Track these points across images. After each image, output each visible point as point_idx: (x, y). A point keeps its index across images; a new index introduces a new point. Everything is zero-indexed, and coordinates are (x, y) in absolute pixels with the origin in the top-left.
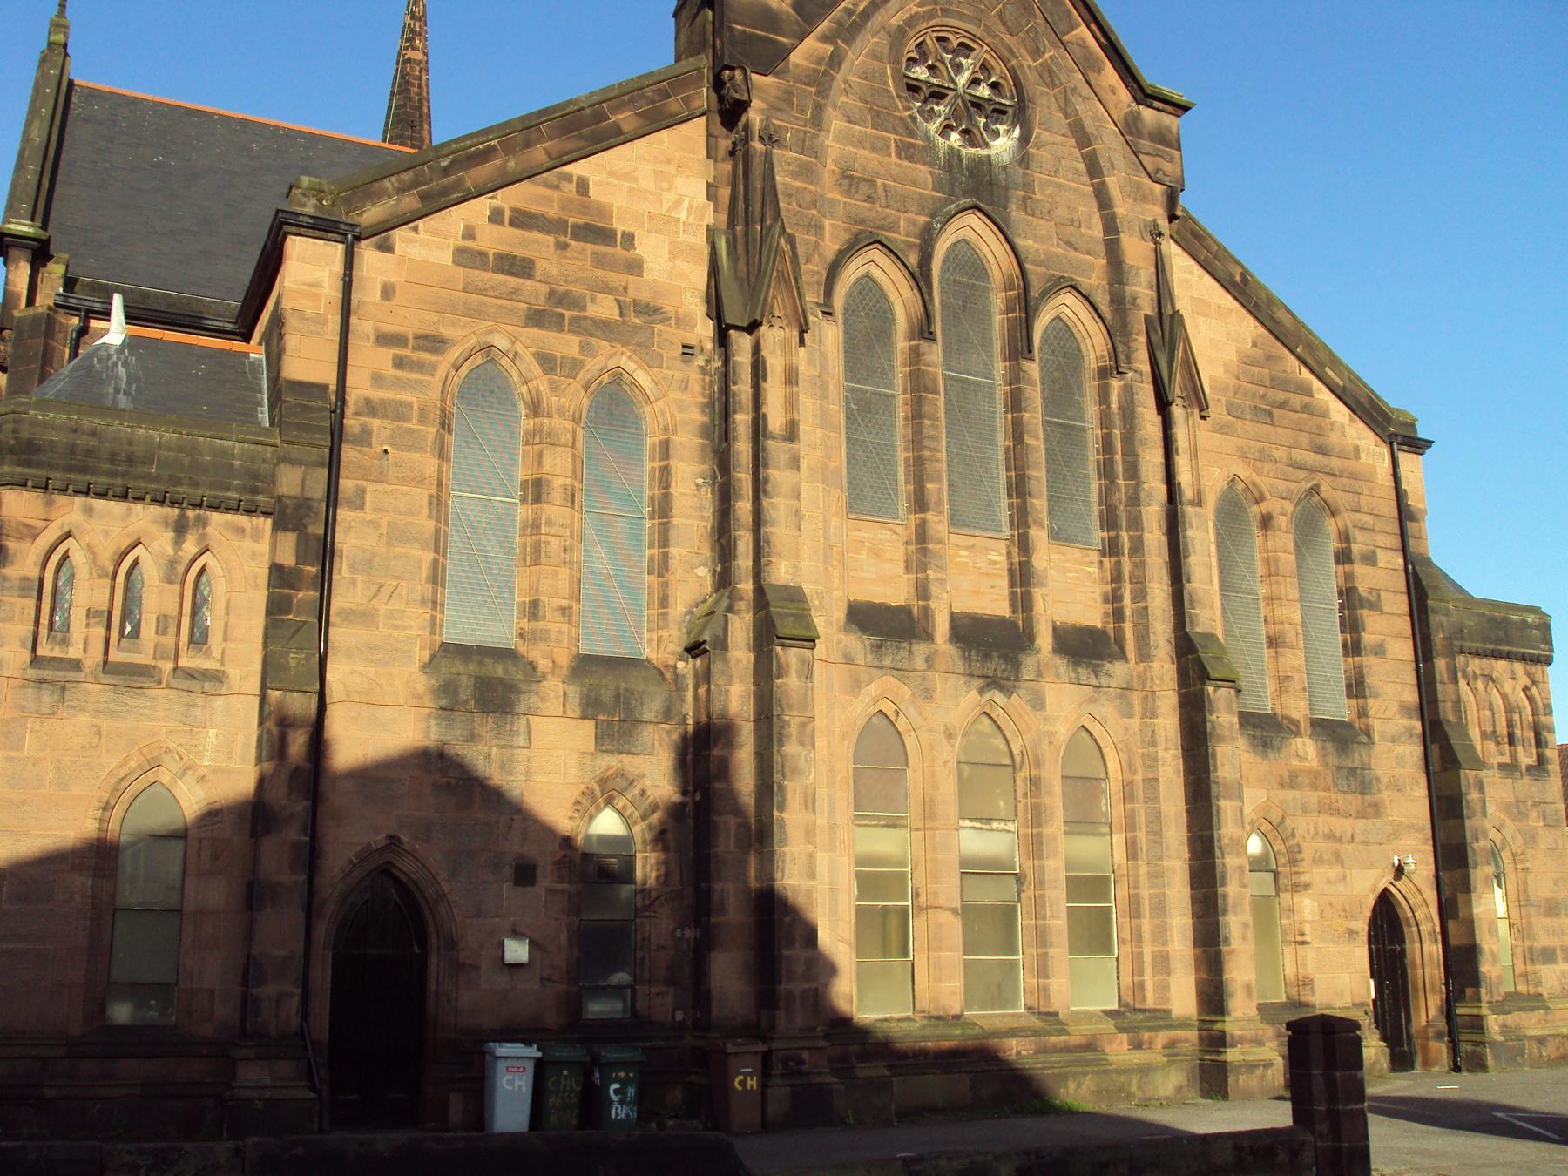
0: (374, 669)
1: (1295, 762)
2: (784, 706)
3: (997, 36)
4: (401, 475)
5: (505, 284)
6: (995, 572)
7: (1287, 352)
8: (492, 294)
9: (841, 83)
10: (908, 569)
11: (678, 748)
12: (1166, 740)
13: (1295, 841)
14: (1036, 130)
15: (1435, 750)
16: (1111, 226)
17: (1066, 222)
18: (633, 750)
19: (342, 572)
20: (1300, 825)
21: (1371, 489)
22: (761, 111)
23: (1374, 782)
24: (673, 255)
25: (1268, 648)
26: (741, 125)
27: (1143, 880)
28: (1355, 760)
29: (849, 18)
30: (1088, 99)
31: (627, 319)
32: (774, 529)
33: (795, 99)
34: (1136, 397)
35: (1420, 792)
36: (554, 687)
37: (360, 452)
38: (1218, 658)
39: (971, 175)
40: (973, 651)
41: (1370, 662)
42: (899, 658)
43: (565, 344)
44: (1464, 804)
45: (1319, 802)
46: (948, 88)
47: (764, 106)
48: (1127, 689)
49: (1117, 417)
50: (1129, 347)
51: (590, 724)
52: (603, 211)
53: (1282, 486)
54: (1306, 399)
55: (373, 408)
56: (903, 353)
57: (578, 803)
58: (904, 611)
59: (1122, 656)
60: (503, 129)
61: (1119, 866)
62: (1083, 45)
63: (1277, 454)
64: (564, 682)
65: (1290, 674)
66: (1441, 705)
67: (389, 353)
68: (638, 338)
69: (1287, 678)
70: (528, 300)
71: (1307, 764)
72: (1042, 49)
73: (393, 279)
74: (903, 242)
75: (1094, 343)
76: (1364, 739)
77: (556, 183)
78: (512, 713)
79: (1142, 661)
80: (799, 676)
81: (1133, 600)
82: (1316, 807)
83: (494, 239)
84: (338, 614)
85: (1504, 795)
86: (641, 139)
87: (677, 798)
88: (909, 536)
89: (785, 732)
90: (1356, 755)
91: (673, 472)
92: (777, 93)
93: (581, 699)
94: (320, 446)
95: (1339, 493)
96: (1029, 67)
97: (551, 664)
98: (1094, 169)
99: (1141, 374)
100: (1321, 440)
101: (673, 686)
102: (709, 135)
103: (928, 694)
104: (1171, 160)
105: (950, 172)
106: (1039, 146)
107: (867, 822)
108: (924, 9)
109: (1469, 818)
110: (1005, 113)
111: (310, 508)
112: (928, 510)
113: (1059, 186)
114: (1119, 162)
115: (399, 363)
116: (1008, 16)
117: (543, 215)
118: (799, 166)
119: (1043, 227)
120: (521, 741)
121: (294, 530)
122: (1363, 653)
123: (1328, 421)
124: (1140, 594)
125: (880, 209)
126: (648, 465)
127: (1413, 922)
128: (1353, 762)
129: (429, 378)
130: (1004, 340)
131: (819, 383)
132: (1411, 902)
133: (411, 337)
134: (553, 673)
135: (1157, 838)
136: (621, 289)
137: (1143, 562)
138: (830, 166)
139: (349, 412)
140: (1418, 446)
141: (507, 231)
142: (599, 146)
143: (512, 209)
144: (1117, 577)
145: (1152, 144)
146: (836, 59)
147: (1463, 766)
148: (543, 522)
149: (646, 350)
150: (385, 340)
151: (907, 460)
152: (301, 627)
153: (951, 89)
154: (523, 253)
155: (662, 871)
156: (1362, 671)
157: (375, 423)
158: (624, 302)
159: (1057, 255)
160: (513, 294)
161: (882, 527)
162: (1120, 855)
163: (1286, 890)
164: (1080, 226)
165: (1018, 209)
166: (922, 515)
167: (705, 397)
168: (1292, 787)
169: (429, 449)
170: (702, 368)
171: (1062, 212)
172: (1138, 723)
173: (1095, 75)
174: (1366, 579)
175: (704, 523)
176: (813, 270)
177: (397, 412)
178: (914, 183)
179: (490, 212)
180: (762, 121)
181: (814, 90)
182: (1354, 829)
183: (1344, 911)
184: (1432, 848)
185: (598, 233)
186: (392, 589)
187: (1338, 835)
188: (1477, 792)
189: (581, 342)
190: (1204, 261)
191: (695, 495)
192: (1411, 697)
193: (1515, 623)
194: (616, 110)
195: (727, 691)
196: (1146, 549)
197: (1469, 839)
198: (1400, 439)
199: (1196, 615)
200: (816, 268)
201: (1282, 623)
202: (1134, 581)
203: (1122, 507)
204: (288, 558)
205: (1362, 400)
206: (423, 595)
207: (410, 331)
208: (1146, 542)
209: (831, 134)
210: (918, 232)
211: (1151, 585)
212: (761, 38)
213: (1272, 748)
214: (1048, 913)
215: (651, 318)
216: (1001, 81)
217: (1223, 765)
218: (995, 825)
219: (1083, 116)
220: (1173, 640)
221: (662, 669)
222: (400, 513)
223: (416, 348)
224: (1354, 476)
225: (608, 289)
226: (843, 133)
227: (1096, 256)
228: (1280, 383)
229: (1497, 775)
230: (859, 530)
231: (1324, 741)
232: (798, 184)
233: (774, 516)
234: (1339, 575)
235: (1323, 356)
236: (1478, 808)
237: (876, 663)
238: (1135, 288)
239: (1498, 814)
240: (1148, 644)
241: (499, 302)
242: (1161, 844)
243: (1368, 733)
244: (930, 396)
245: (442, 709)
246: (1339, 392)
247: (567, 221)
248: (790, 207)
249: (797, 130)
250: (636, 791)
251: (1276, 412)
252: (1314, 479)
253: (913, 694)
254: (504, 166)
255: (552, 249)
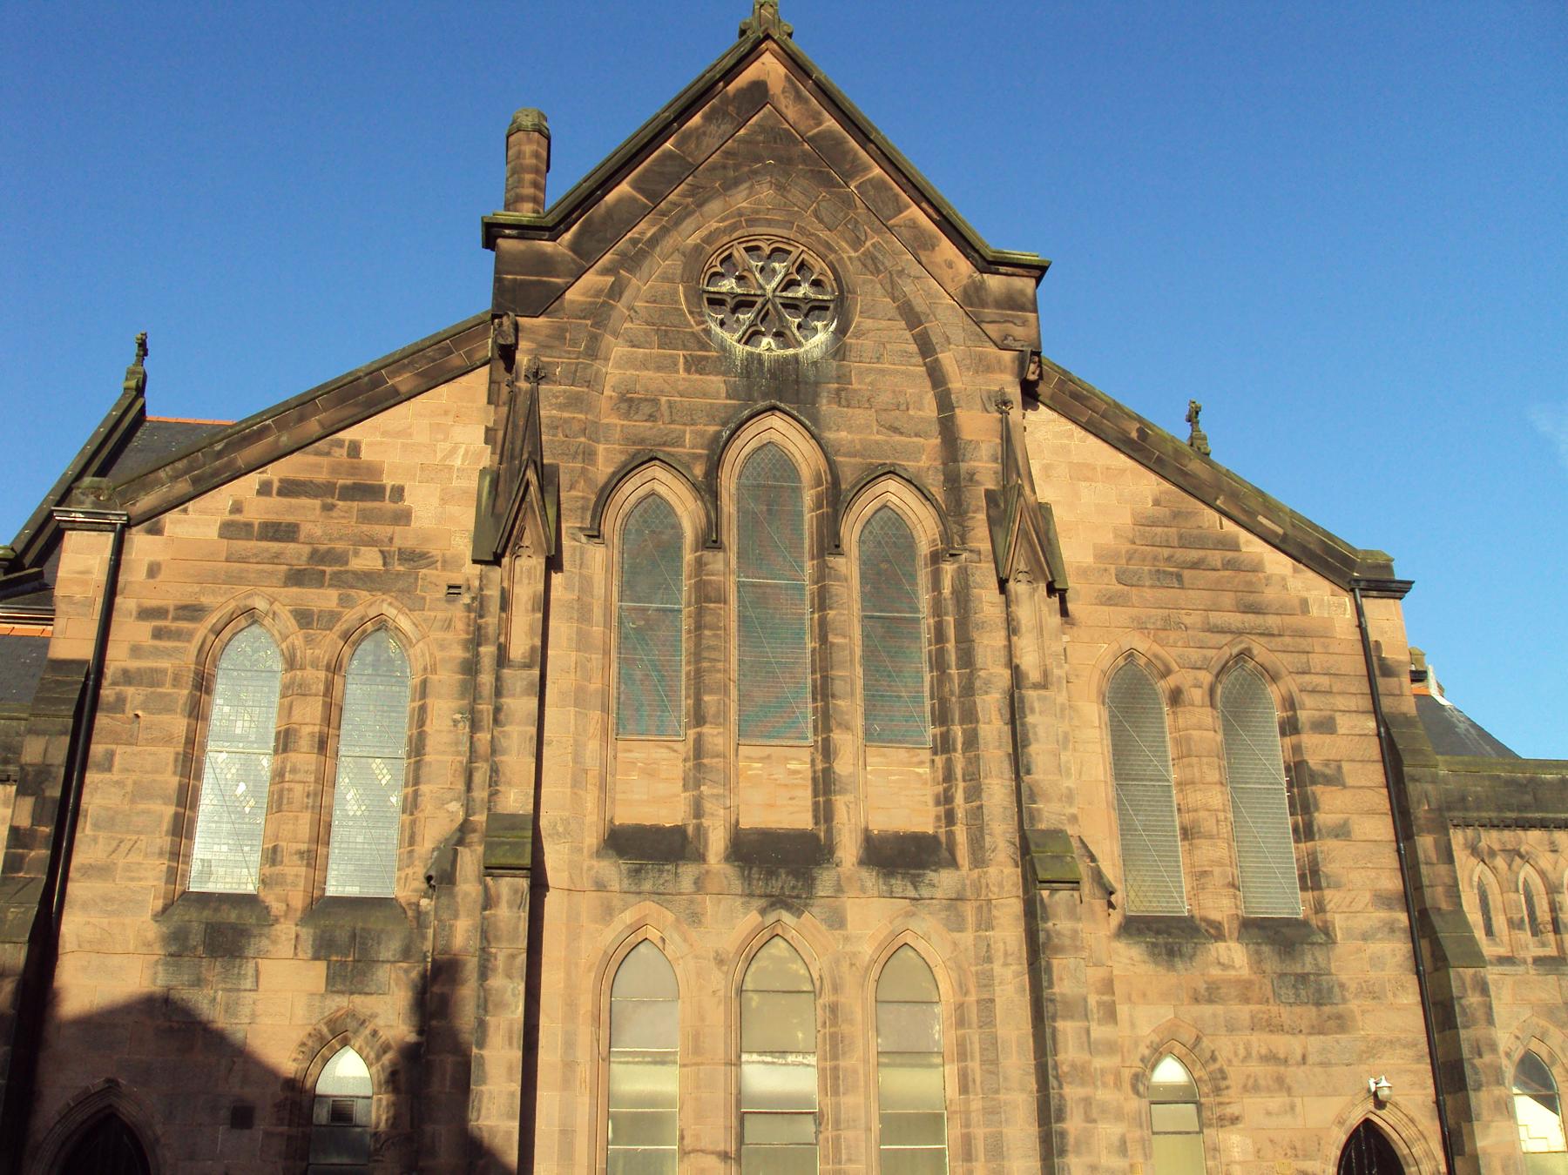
0: (106, 920)
1: (1216, 972)
2: (491, 939)
3: (812, 234)
4: (149, 736)
5: (267, 550)
6: (795, 781)
7: (1204, 506)
8: (255, 561)
9: (625, 311)
10: (685, 788)
11: (416, 986)
12: (1006, 954)
13: (1217, 1066)
14: (857, 319)
15: (1424, 944)
16: (945, 404)
17: (891, 407)
18: (367, 990)
19: (85, 831)
20: (1224, 1046)
21: (1326, 646)
22: (530, 352)
23: (1336, 990)
24: (443, 501)
25: (1183, 840)
26: (514, 371)
27: (975, 1117)
28: (1307, 964)
29: (635, 247)
30: (918, 278)
31: (390, 567)
32: (503, 758)
33: (568, 335)
34: (971, 579)
35: (1410, 998)
36: (286, 930)
37: (112, 718)
38: (1057, 857)
39: (773, 376)
40: (755, 870)
41: (1326, 846)
42: (661, 881)
43: (324, 599)
44: (1457, 1008)
45: (1252, 1017)
46: (755, 295)
47: (533, 346)
48: (956, 899)
49: (949, 602)
50: (964, 527)
51: (321, 967)
52: (373, 469)
53: (1195, 655)
54: (1230, 555)
55: (129, 677)
56: (689, 565)
57: (303, 1044)
58: (679, 831)
59: (953, 863)
60: (286, 407)
61: (951, 1101)
62: (913, 225)
63: (1188, 620)
64: (297, 925)
65: (1207, 869)
66: (1427, 892)
67: (147, 627)
68: (400, 585)
69: (1204, 873)
70: (289, 562)
71: (1233, 973)
72: (863, 238)
73: (160, 558)
74: (688, 454)
75: (925, 526)
76: (1321, 938)
77: (326, 450)
78: (241, 957)
79: (976, 867)
80: (510, 906)
81: (967, 799)
82: (1247, 1023)
83: (259, 510)
84: (78, 870)
85: (1544, 996)
86: (418, 397)
87: (412, 1037)
88: (687, 752)
89: (490, 966)
90: (1308, 959)
91: (429, 710)
92: (546, 331)
93: (314, 940)
94: (63, 717)
95: (1280, 655)
96: (850, 258)
97: (284, 907)
98: (926, 347)
99: (979, 553)
100: (1251, 598)
101: (414, 924)
102: (492, 382)
103: (695, 918)
104: (1025, 323)
105: (748, 378)
106: (857, 336)
107: (630, 1059)
108: (726, 223)
109: (1466, 1027)
110: (827, 308)
111: (49, 773)
112: (705, 723)
113: (882, 371)
114: (957, 334)
115: (158, 634)
116: (823, 213)
117: (311, 482)
118: (568, 398)
119: (860, 416)
120: (248, 984)
121: (32, 795)
122: (1317, 837)
123: (1261, 575)
124: (974, 792)
125: (662, 427)
126: (684, 669)
127: (1410, 1160)
128: (1303, 966)
129: (186, 644)
130: (812, 538)
131: (576, 607)
132: (1403, 1135)
133: (171, 609)
134: (286, 915)
135: (991, 1068)
136: (386, 540)
137: (977, 757)
138: (608, 392)
139: (105, 683)
140: (1388, 586)
141: (275, 501)
142: (372, 411)
143: (281, 481)
144: (949, 776)
145: (1000, 311)
146: (616, 288)
147: (1452, 962)
148: (288, 769)
149: (409, 597)
150: (145, 614)
151: (688, 674)
152: (28, 883)
153: (759, 296)
154: (290, 519)
155: (391, 1113)
156: (1317, 857)
157: (130, 691)
158: (389, 552)
159: (877, 442)
160: (275, 559)
161: (658, 746)
162: (952, 1090)
163: (1210, 1125)
164: (908, 409)
165: (829, 402)
166: (698, 729)
167: (468, 633)
168: (1210, 1001)
169: (179, 710)
170: (468, 605)
171: (884, 398)
172: (972, 937)
173: (927, 253)
174: (1317, 750)
175: (459, 758)
176: (574, 496)
177: (150, 678)
178: (705, 395)
179: (260, 486)
180: (530, 360)
181: (589, 322)
182: (1305, 1048)
183: (1295, 1148)
184: (1430, 1067)
185: (366, 490)
186: (132, 843)
187: (1282, 1056)
188: (1477, 994)
189: (340, 595)
190: (1087, 422)
191: (450, 732)
192: (1391, 882)
193: (1550, 784)
194: (393, 374)
195: (451, 926)
196: (981, 741)
197: (1466, 1053)
198: (1362, 584)
199: (1038, 810)
200: (580, 494)
201: (1196, 811)
202: (967, 778)
203: (954, 699)
204: (24, 821)
205: (1312, 546)
206: (161, 848)
207: (170, 603)
208: (981, 734)
209: (611, 362)
210: (706, 442)
211: (987, 781)
212: (532, 282)
213: (1181, 955)
214: (844, 1157)
215: (416, 564)
216: (821, 277)
217: (1061, 979)
218: (791, 1058)
219: (911, 297)
220: (1017, 840)
221: (406, 907)
222: (147, 772)
223: (176, 619)
224: (1302, 634)
225: (372, 542)
226: (624, 358)
227: (926, 436)
228: (1200, 542)
229: (1532, 972)
230: (630, 751)
231: (1258, 944)
232: (566, 415)
233: (505, 745)
234: (1285, 746)
235: (1253, 504)
236: (1480, 1014)
237: (634, 888)
238: (973, 464)
239: (1535, 1020)
240: (982, 848)
241: (260, 567)
242: (997, 1074)
243: (1327, 930)
244: (712, 605)
245: (171, 955)
246: (1277, 541)
247: (336, 484)
248: (555, 439)
249: (570, 364)
250: (367, 1032)
251: (1187, 573)
252: (1241, 642)
253: (677, 920)
254: (277, 441)
255: (318, 512)
